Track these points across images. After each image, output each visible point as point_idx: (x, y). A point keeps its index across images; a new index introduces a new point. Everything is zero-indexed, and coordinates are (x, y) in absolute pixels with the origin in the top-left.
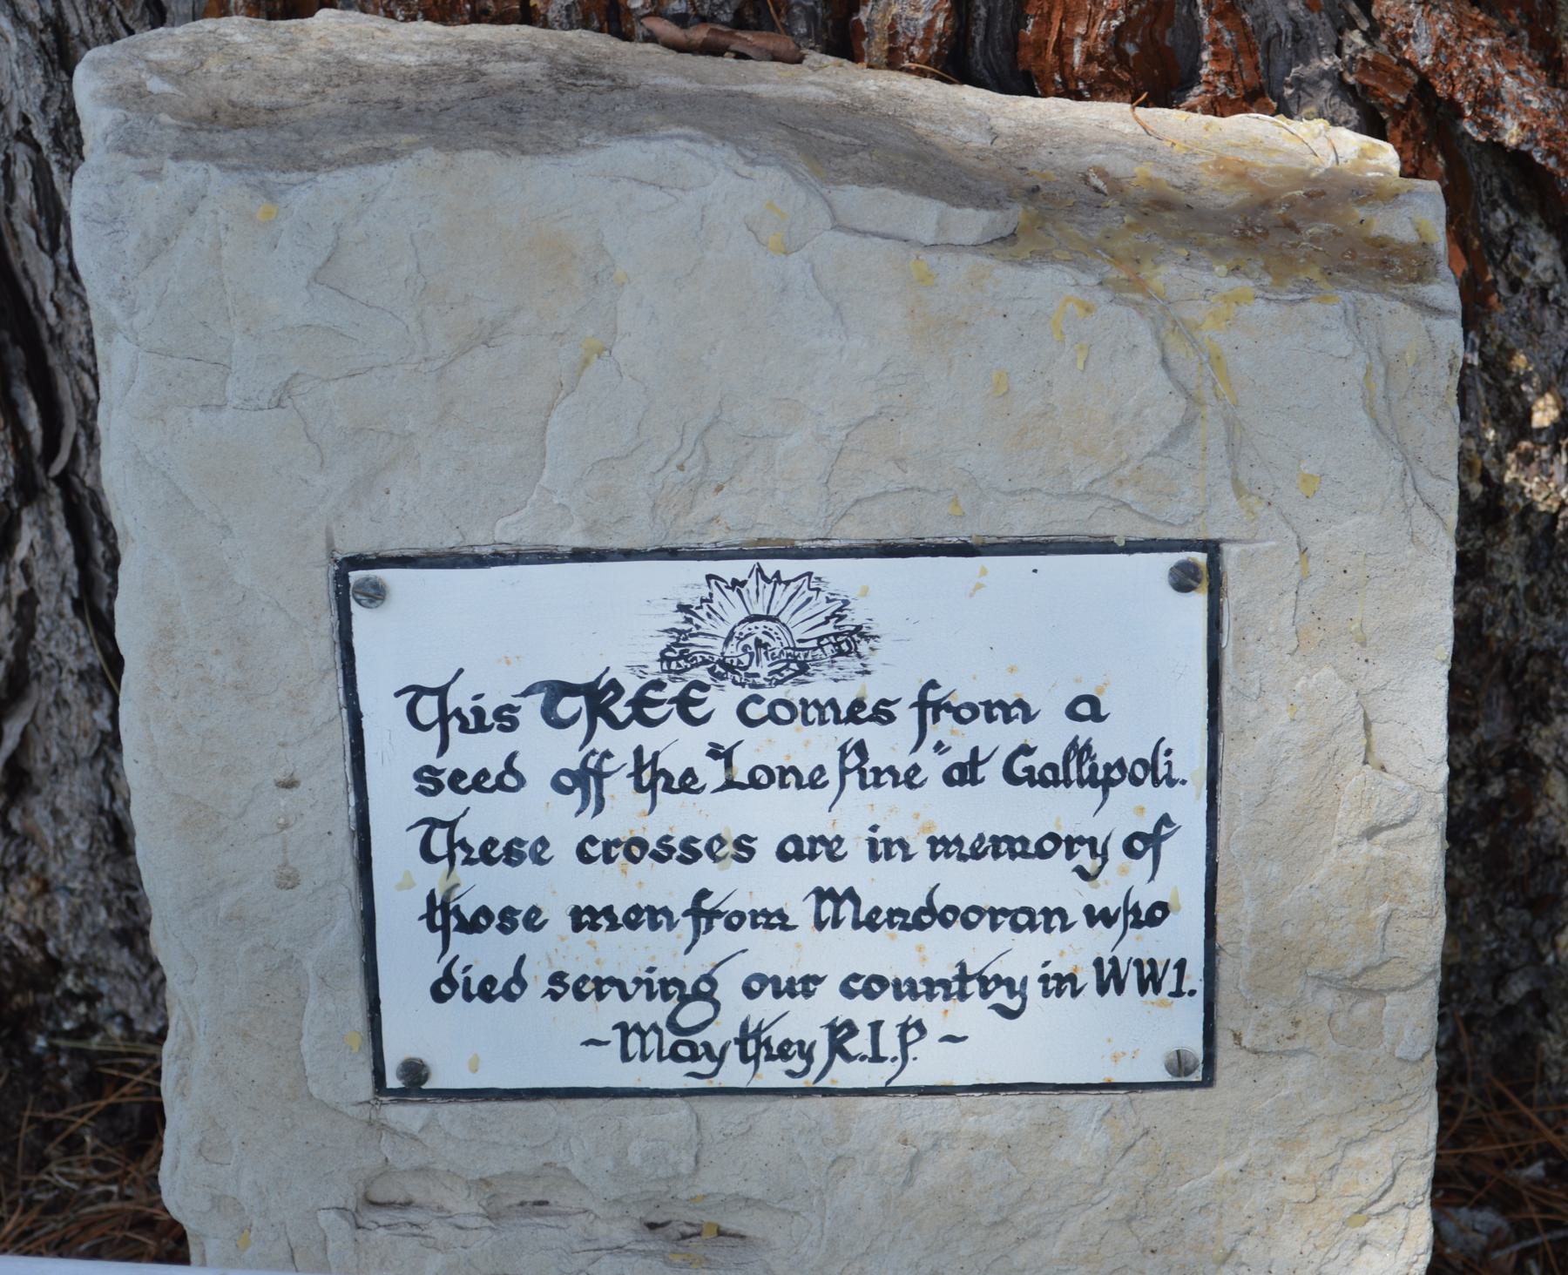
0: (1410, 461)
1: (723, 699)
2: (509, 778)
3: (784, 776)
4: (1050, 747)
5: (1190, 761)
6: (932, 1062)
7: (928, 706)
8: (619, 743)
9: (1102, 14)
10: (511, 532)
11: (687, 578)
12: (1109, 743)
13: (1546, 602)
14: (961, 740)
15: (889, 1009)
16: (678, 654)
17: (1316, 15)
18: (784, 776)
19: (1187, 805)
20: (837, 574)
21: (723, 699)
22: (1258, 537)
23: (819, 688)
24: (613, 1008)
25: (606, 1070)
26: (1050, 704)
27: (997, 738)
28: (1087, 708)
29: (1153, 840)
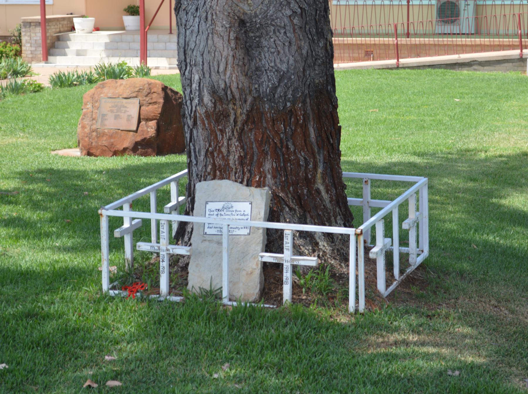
0: (263, 199)
1: (225, 210)
2: (213, 215)
3: (228, 215)
4: (242, 213)
5: (250, 214)
6: (234, 233)
7: (236, 211)
8: (219, 213)
9: (100, 371)
10: (215, 200)
11: (224, 203)
12: (246, 213)
13: (214, 128)
14: (237, 213)
15: (232, 229)
16: (223, 207)
17: (450, 200)
18: (228, 215)
19: (249, 217)
20: (232, 203)
21: (225, 210)
22: (215, 37)
23: (230, 210)
24: (217, 229)
25: (216, 233)
26: (242, 211)
27: (239, 213)
28: (244, 211)
29: (247, 219)
